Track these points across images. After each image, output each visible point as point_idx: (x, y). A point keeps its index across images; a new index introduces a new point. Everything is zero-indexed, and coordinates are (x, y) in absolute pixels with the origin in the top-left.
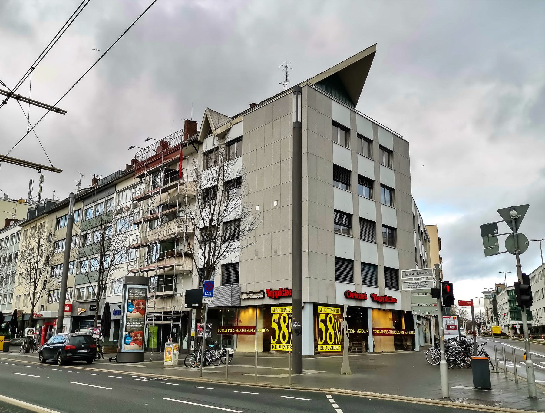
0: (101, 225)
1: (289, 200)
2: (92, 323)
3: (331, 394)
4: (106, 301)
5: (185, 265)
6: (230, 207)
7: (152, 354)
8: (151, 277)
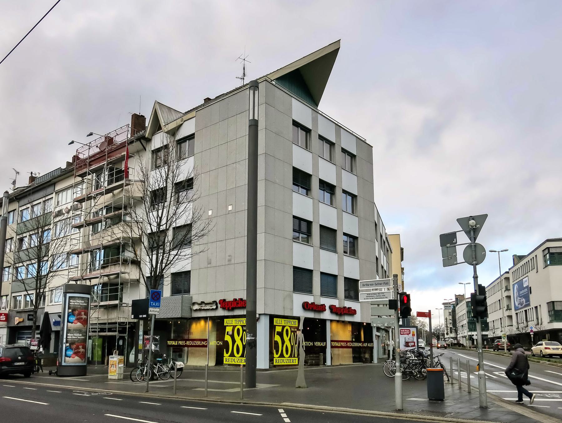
0: (38, 228)
1: (244, 205)
2: (30, 334)
3: (284, 409)
4: (45, 311)
5: (132, 273)
6: (179, 211)
7: (96, 367)
8: (94, 286)
